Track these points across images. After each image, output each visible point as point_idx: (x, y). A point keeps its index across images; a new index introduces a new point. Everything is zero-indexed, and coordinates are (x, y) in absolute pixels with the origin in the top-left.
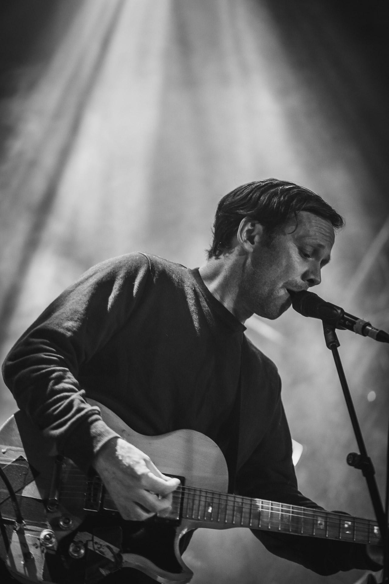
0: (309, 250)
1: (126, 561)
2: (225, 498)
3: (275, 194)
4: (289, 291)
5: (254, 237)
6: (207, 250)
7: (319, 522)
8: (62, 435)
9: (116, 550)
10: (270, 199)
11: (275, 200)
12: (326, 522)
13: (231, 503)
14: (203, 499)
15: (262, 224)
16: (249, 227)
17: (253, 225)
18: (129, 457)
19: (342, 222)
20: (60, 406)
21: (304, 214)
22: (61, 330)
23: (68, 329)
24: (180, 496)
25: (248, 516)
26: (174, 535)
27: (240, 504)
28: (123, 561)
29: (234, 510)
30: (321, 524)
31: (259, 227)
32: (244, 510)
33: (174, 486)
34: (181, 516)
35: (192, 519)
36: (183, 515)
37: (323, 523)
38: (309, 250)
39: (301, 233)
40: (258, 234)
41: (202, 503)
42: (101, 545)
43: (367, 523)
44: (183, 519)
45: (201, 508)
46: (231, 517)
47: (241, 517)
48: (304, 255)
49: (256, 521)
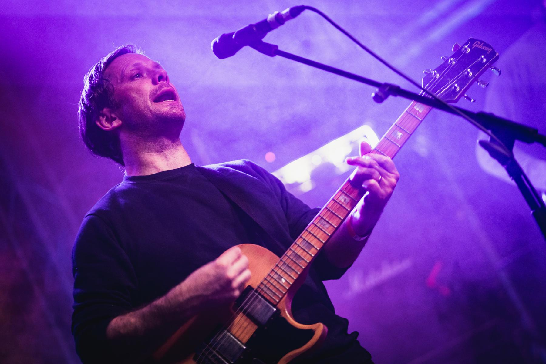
2: (282, 263)
5: (111, 117)
8: (285, 321)
18: (107, 81)
24: (260, 297)
25: (305, 253)
30: (345, 200)
32: (299, 254)
33: (366, 124)
34: (275, 306)
36: (275, 303)
37: (346, 197)
39: (119, 77)
43: (340, 193)
46: (298, 267)
47: (303, 259)
49: (313, 249)
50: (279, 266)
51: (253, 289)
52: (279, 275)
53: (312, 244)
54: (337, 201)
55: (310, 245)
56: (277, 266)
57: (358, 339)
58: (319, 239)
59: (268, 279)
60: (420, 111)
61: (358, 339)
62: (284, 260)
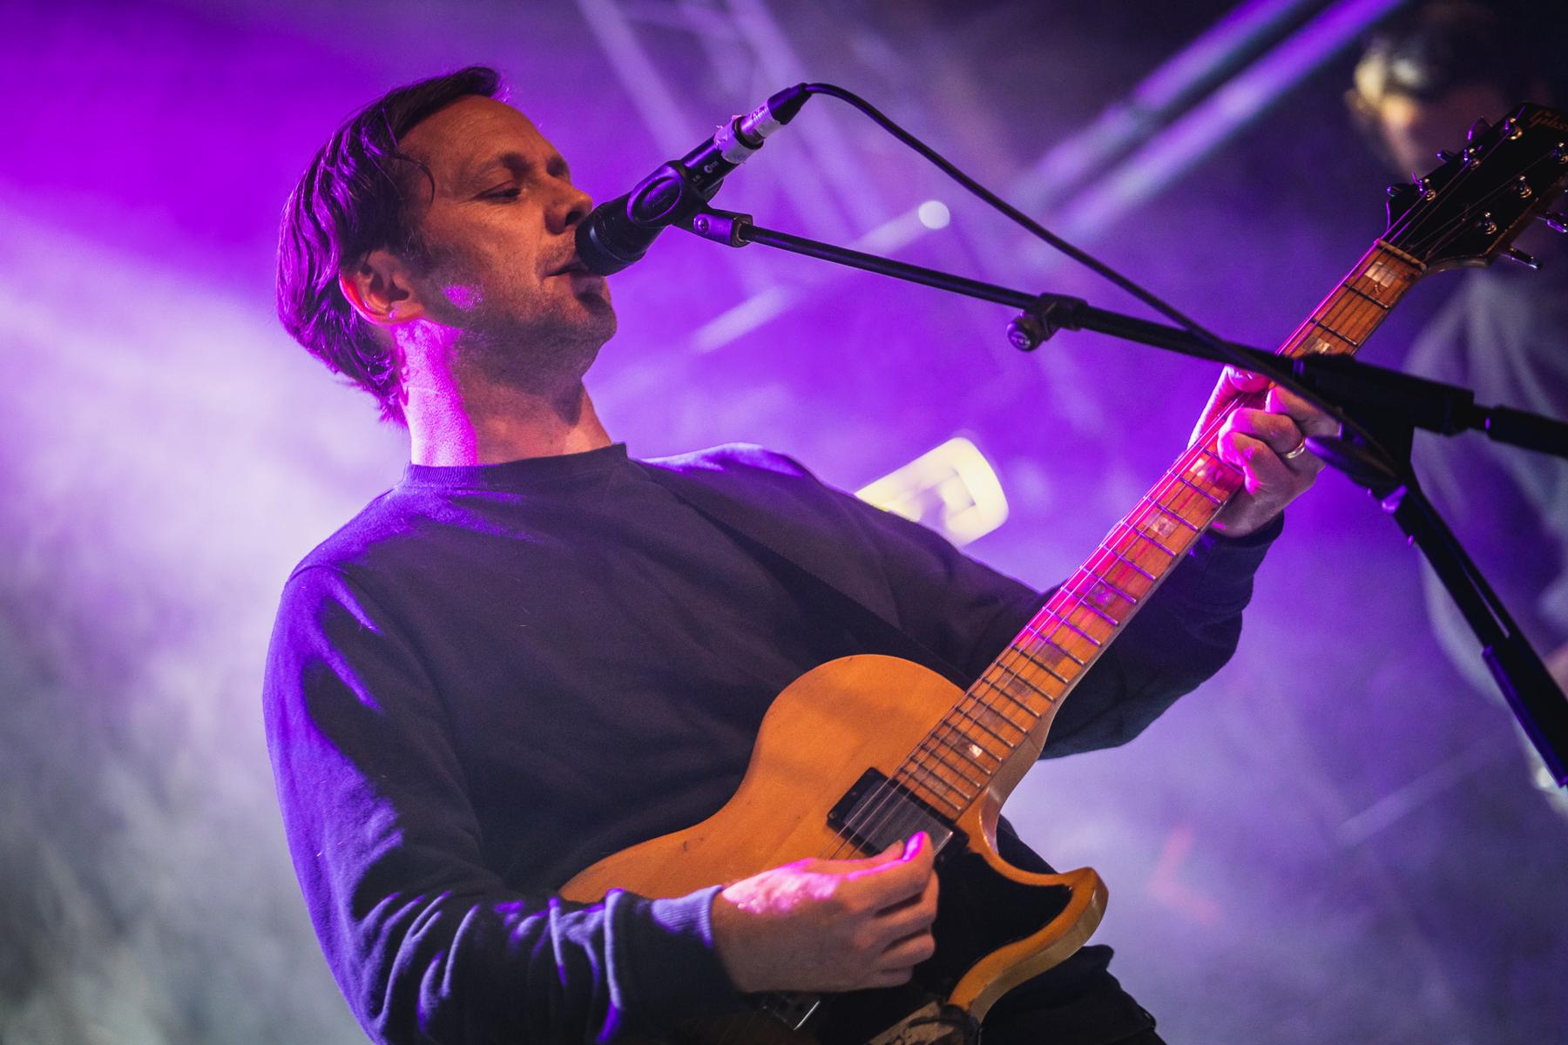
0: (500, 177)
1: (971, 1004)
3: (327, 180)
4: (559, 273)
6: (383, 418)
7: (1155, 528)
9: (930, 1010)
10: (332, 202)
11: (340, 190)
12: (1164, 512)
13: (991, 698)
14: (943, 751)
15: (378, 248)
16: (364, 282)
17: (367, 271)
19: (489, 70)
20: (416, 931)
21: (415, 139)
22: (376, 853)
23: (383, 835)
26: (979, 861)
27: (1007, 675)
28: (966, 1008)
29: (1011, 699)
30: (1162, 527)
31: (378, 258)
32: (1023, 676)
35: (972, 801)
36: (952, 815)
38: (500, 177)
39: (449, 172)
40: (392, 270)
41: (952, 758)
42: (899, 1037)
44: (959, 823)
45: (962, 765)
48: (508, 196)
49: (1066, 662)
50: (965, 709)
51: (885, 778)
52: (964, 736)
53: (1065, 647)
54: (1358, 287)
55: (1058, 653)
56: (957, 710)
57: (1111, 970)
58: (1083, 635)
59: (954, 721)
60: (1385, 284)
61: (1111, 970)
62: (978, 694)
